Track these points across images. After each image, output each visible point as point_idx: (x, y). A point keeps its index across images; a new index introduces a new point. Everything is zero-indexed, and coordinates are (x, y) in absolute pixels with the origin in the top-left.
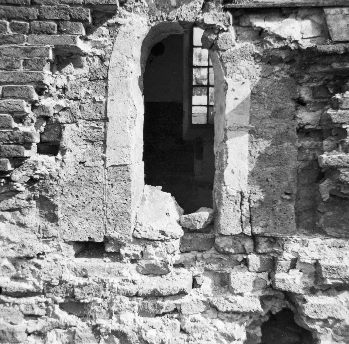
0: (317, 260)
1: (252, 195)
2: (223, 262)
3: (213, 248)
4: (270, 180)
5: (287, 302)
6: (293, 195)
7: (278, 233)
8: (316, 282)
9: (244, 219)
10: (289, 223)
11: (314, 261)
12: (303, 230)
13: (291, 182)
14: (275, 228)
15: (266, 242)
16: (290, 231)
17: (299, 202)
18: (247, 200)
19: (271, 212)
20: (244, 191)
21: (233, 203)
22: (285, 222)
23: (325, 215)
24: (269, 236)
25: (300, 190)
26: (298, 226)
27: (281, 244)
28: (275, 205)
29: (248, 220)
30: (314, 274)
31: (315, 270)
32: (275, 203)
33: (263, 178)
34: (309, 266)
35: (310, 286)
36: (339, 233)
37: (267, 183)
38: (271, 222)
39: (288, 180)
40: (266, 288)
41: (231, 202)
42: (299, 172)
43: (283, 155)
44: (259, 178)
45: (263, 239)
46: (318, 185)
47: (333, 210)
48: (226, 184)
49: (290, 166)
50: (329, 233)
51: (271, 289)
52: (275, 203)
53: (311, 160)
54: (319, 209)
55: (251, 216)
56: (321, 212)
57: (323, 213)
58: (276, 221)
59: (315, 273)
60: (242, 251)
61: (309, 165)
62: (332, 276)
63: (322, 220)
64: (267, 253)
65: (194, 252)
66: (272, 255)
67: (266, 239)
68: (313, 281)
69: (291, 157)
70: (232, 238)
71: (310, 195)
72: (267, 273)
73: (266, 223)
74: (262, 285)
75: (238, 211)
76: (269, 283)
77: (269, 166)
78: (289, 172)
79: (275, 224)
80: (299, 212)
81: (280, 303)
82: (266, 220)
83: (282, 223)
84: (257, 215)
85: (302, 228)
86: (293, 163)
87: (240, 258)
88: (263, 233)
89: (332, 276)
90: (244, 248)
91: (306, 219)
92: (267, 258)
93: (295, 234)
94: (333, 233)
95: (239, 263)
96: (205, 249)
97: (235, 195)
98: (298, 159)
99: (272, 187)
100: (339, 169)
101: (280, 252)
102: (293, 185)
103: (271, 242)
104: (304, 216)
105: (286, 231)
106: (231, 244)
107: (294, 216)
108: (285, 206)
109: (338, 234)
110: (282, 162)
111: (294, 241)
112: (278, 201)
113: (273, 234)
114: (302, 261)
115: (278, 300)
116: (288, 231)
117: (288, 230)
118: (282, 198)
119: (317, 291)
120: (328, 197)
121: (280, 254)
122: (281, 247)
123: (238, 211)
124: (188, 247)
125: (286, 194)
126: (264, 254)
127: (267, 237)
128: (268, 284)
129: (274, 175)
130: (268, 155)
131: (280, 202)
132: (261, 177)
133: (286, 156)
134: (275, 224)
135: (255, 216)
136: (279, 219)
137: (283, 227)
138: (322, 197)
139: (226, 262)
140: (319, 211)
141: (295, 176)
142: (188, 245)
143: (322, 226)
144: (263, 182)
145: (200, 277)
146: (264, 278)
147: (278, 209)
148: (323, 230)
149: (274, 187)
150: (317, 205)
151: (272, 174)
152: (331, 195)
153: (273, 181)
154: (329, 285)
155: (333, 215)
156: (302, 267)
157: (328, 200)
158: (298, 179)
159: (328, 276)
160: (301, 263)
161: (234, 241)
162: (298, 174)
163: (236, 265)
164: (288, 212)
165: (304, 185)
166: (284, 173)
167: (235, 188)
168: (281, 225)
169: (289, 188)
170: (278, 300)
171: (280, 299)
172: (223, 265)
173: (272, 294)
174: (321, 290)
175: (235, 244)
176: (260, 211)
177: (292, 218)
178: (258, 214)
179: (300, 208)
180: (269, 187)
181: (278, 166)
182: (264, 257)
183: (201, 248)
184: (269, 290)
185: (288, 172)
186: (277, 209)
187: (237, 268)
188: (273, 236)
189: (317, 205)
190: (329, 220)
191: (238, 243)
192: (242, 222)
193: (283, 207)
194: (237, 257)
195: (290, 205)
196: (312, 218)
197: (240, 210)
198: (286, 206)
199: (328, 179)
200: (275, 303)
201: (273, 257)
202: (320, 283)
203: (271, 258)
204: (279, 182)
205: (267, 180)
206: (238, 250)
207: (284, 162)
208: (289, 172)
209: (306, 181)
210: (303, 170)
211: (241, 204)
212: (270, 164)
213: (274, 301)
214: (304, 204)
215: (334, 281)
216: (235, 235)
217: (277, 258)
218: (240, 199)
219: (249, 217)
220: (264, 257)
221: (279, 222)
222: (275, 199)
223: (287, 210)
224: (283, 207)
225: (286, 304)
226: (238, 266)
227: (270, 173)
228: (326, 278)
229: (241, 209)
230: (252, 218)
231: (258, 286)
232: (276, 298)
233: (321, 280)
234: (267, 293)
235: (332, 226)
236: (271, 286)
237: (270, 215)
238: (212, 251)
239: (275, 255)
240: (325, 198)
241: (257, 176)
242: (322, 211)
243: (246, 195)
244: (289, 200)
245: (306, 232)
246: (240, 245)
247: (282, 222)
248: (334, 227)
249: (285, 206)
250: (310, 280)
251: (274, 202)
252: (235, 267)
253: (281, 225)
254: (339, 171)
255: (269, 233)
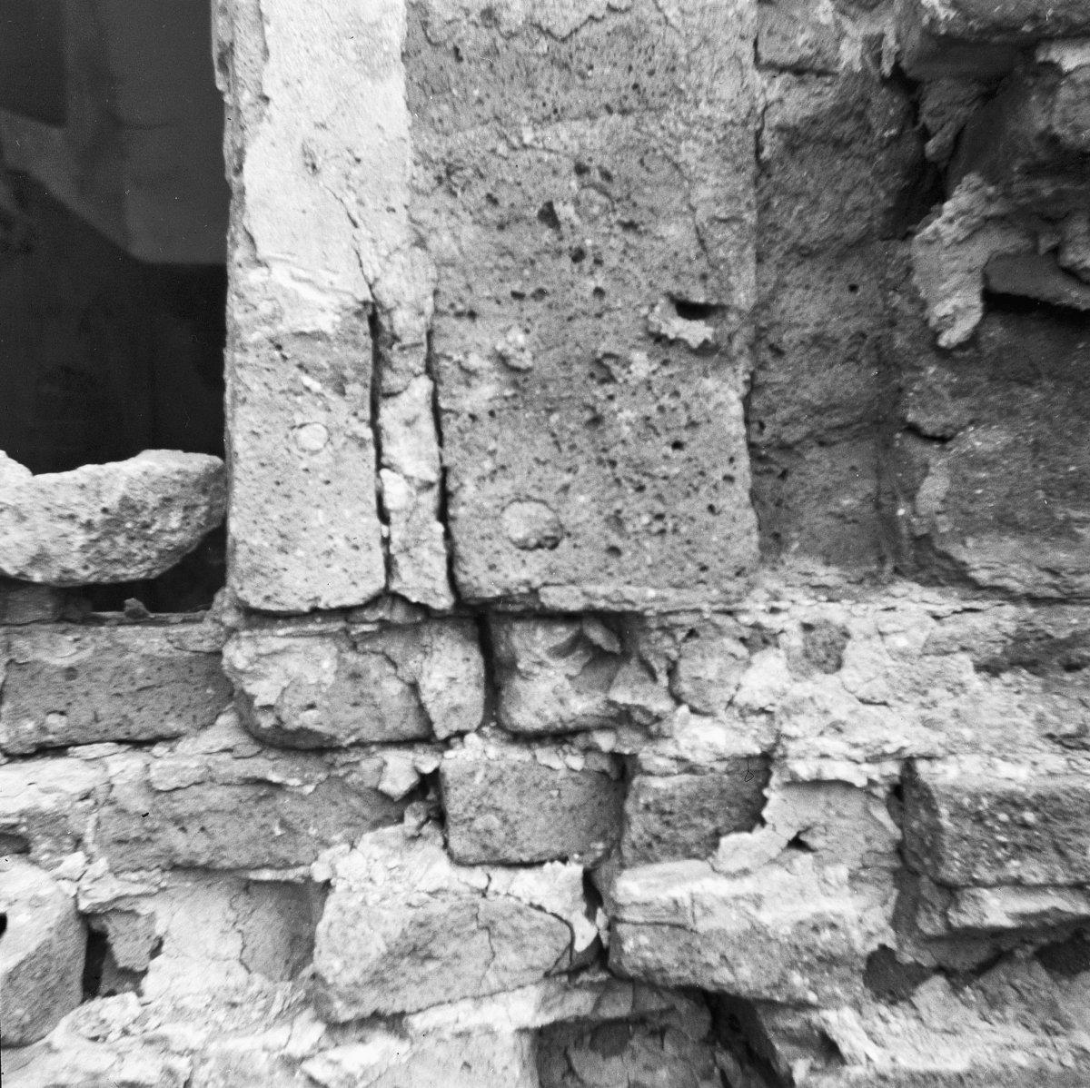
0: (908, 764)
1: (448, 324)
2: (284, 802)
3: (222, 720)
4: (565, 211)
5: (726, 1060)
6: (732, 317)
7: (645, 582)
8: (902, 919)
9: (397, 494)
10: (711, 508)
11: (892, 768)
12: (807, 564)
13: (714, 220)
14: (614, 551)
15: (561, 652)
16: (717, 567)
17: (777, 375)
18: (416, 363)
19: (582, 441)
20: (388, 300)
21: (316, 386)
22: (682, 507)
23: (955, 449)
24: (575, 605)
25: (781, 285)
26: (773, 542)
27: (659, 665)
28: (610, 388)
29: (430, 500)
30: (896, 864)
31: (897, 834)
32: (609, 379)
33: (518, 198)
34: (854, 805)
35: (863, 947)
36: (1054, 572)
37: (547, 235)
38: (581, 509)
39: (693, 209)
40: (574, 972)
41: (307, 380)
42: (766, 154)
43: (657, 30)
44: (492, 200)
45: (540, 633)
46: (902, 251)
47: (1008, 414)
48: (264, 251)
49: (704, 109)
50: (983, 576)
51: (603, 976)
52: (609, 379)
53: (852, 75)
54: (911, 417)
55: (445, 471)
56: (929, 430)
57: (943, 440)
58: (618, 505)
59: (900, 849)
60: (411, 727)
61: (841, 111)
62: (1013, 868)
63: (934, 488)
64: (575, 732)
65: (99, 749)
66: (605, 741)
67: (562, 634)
68: (889, 910)
69: (706, 41)
70: (334, 636)
71: (852, 326)
72: (575, 870)
73: (549, 516)
74: (545, 952)
75: (362, 444)
76: (585, 934)
77: (558, 114)
78: (700, 151)
79: (617, 521)
80: (785, 448)
81: (680, 1070)
82: (549, 496)
83: (660, 517)
84: (488, 465)
85: (805, 551)
86: (726, 88)
87: (398, 772)
88: (534, 592)
89: (1013, 868)
90: (421, 708)
91: (826, 493)
92: (577, 762)
93: (968, 983)
94: (1014, 569)
95: (389, 808)
96: (172, 725)
97: (329, 330)
98: (757, 58)
99: (587, 263)
100: (1054, 55)
101: (658, 719)
102: (726, 243)
103: (598, 657)
104: (818, 467)
105: (691, 568)
106: (329, 679)
107: (744, 462)
108: (676, 394)
109: (1047, 578)
110: (645, 81)
111: (746, 633)
112: (626, 364)
113: (604, 592)
114: (804, 770)
115: (670, 1049)
116: (704, 569)
117: (701, 557)
118: (659, 338)
119: (918, 975)
120: (975, 317)
121: (650, 727)
122: (663, 680)
123: (362, 444)
124: (55, 721)
125: (688, 310)
126: (559, 736)
127: (568, 617)
128: (581, 945)
129: (596, 176)
130: (548, 33)
131: (641, 365)
132: (503, 194)
133: (672, 38)
134: (617, 521)
135: (477, 472)
136: (641, 489)
137: (670, 539)
138: (933, 322)
139: (304, 809)
140: (913, 430)
141: (741, 182)
142: (51, 702)
143: (934, 526)
144: (522, 228)
145: (133, 914)
146: (554, 905)
147: (628, 414)
148: (946, 556)
149: (598, 262)
150: (900, 390)
151: (581, 170)
152: (994, 302)
153: (593, 220)
154: (997, 933)
155: (1008, 450)
156: (810, 810)
157: (973, 340)
158: (765, 207)
159: (983, 873)
160: (794, 783)
161: (351, 657)
162: (763, 167)
163: (375, 825)
164: (703, 434)
165: (804, 253)
166: (666, 157)
167: (325, 278)
168: (657, 526)
169: (701, 266)
170: (670, 1049)
171: (681, 1040)
172: (283, 824)
173: (618, 1007)
174: (940, 970)
175: (355, 676)
176: (509, 434)
177: (729, 479)
178: (492, 453)
179: (783, 414)
180: (566, 262)
181: (624, 112)
182: (556, 763)
183: (143, 723)
184: (592, 986)
185: (689, 153)
186: (625, 416)
187: (381, 843)
188: (601, 604)
189: (900, 390)
190: (982, 482)
191: (374, 674)
192: (384, 516)
193: (666, 400)
194: (380, 770)
195: (710, 384)
196: (868, 486)
197: (368, 433)
198: (686, 392)
199: (972, 179)
200: (647, 1068)
201: (615, 757)
202: (930, 925)
203: (605, 764)
204: (630, 226)
205: (548, 216)
206: (381, 720)
207: (661, 81)
208: (700, 151)
209: (819, 225)
210: (795, 138)
211: (378, 395)
212: (564, 99)
213: (644, 1058)
214: (812, 391)
215: (1031, 904)
216: (345, 612)
217: (633, 756)
218: (365, 357)
219: (434, 477)
220: (556, 763)
221: (638, 507)
222: (604, 347)
223: (693, 425)
224: (666, 400)
225: (723, 1074)
226: (390, 830)
227: (566, 166)
228: (978, 884)
229: (374, 424)
230: (452, 484)
231: (509, 957)
232: (660, 1033)
233: (939, 900)
234: (579, 1003)
235: (1005, 523)
236: (600, 953)
237: (580, 459)
238: (224, 732)
239: (628, 743)
240: (947, 322)
241: (481, 189)
242: (930, 422)
243: (405, 322)
244: (705, 350)
245: (828, 575)
246: (393, 688)
247: (660, 508)
248: (1018, 528)
249: (676, 394)
250: (862, 901)
251: (603, 368)
252: (368, 836)
253: (657, 526)
254: (1053, 67)
255: (576, 590)
